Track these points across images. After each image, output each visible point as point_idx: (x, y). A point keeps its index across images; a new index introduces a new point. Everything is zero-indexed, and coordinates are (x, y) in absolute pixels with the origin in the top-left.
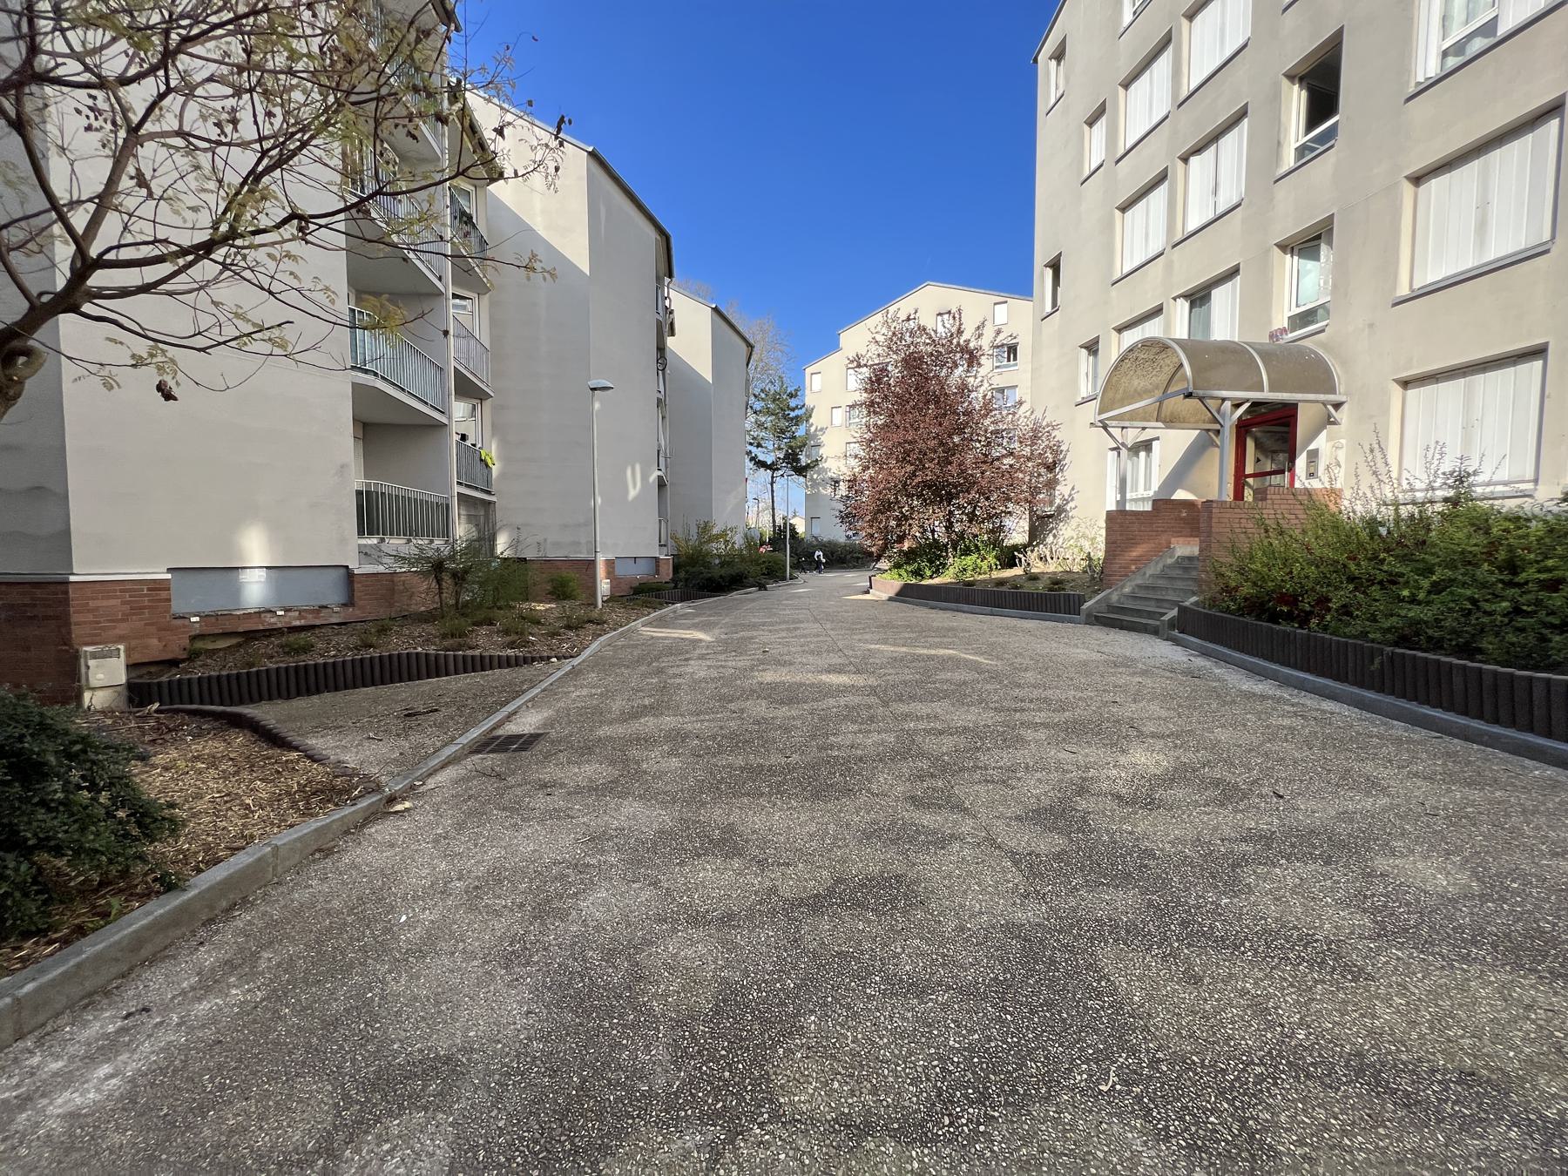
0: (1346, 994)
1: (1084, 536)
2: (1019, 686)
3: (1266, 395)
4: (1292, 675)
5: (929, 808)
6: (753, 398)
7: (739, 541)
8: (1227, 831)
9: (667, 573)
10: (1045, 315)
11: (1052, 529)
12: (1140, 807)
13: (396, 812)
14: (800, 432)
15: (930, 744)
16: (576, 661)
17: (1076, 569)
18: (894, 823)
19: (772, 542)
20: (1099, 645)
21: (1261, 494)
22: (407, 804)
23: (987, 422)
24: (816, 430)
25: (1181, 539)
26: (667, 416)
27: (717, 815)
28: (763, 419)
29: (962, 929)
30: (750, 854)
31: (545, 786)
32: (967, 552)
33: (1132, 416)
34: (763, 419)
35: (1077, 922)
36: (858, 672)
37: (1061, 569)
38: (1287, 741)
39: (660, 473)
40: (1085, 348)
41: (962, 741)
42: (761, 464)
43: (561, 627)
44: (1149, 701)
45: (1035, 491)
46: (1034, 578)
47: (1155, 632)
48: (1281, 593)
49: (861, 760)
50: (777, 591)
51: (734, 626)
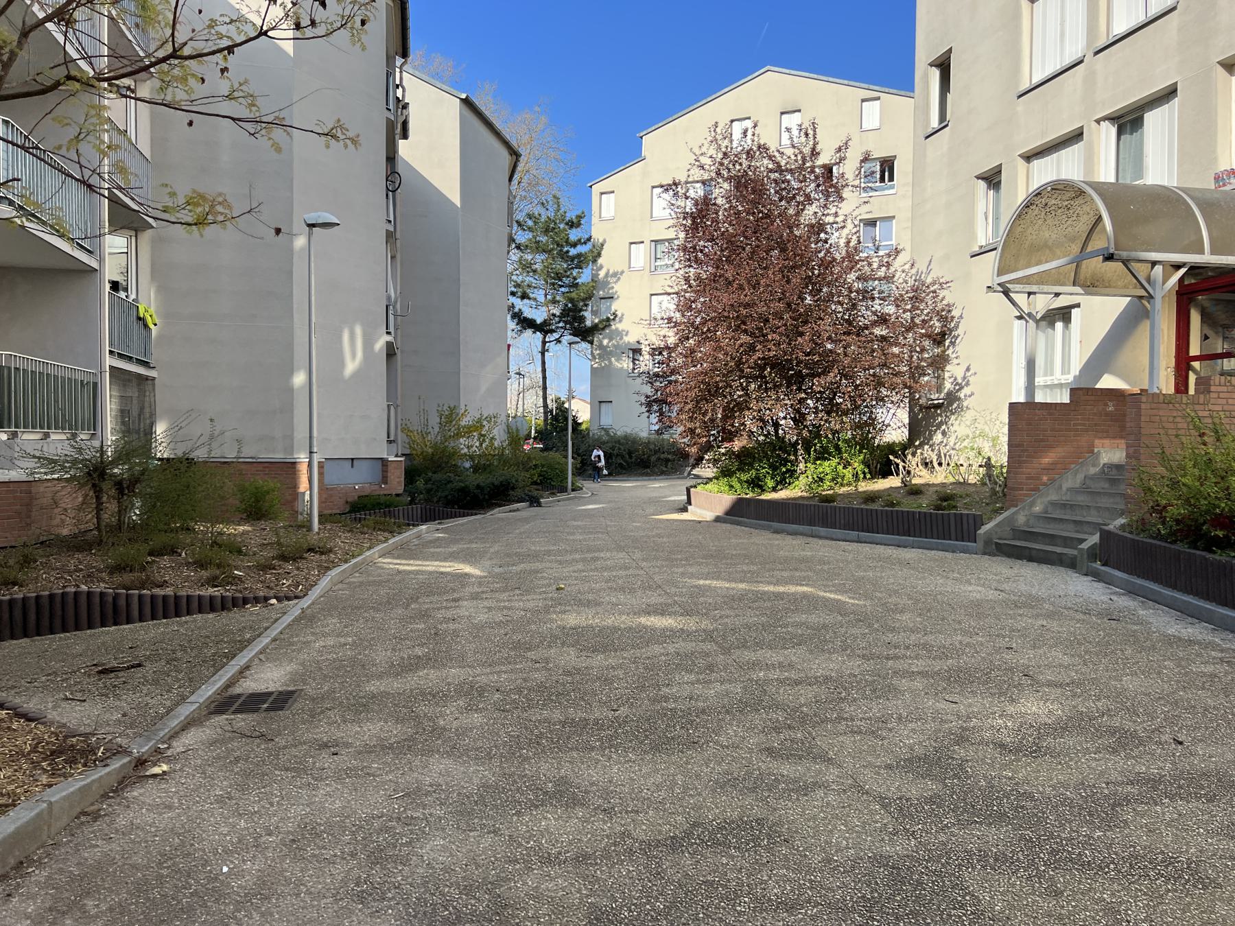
0: (1193, 898)
1: (983, 435)
2: (893, 630)
3: (1207, 258)
4: (1228, 616)
5: (788, 758)
6: (515, 225)
7: (499, 436)
8: (1114, 776)
9: (397, 483)
10: (930, 131)
11: (941, 423)
12: (1025, 755)
13: (155, 776)
14: (584, 277)
15: (785, 695)
16: (305, 603)
17: (972, 479)
18: (749, 774)
19: (542, 435)
20: (999, 581)
21: (1203, 383)
22: (165, 767)
23: (852, 277)
24: (607, 275)
25: (1107, 442)
26: (398, 256)
27: (546, 769)
28: (529, 257)
29: (829, 861)
30: (593, 804)
31: (325, 746)
32: (823, 455)
33: (1042, 279)
34: (529, 257)
35: (946, 853)
36: (687, 613)
37: (952, 480)
38: (1203, 688)
39: (389, 338)
40: (983, 179)
41: (823, 693)
42: (526, 323)
43: (273, 558)
44: (1051, 647)
45: (916, 372)
46: (916, 491)
47: (1071, 564)
48: (1216, 514)
49: (703, 712)
50: (555, 507)
51: (508, 555)
